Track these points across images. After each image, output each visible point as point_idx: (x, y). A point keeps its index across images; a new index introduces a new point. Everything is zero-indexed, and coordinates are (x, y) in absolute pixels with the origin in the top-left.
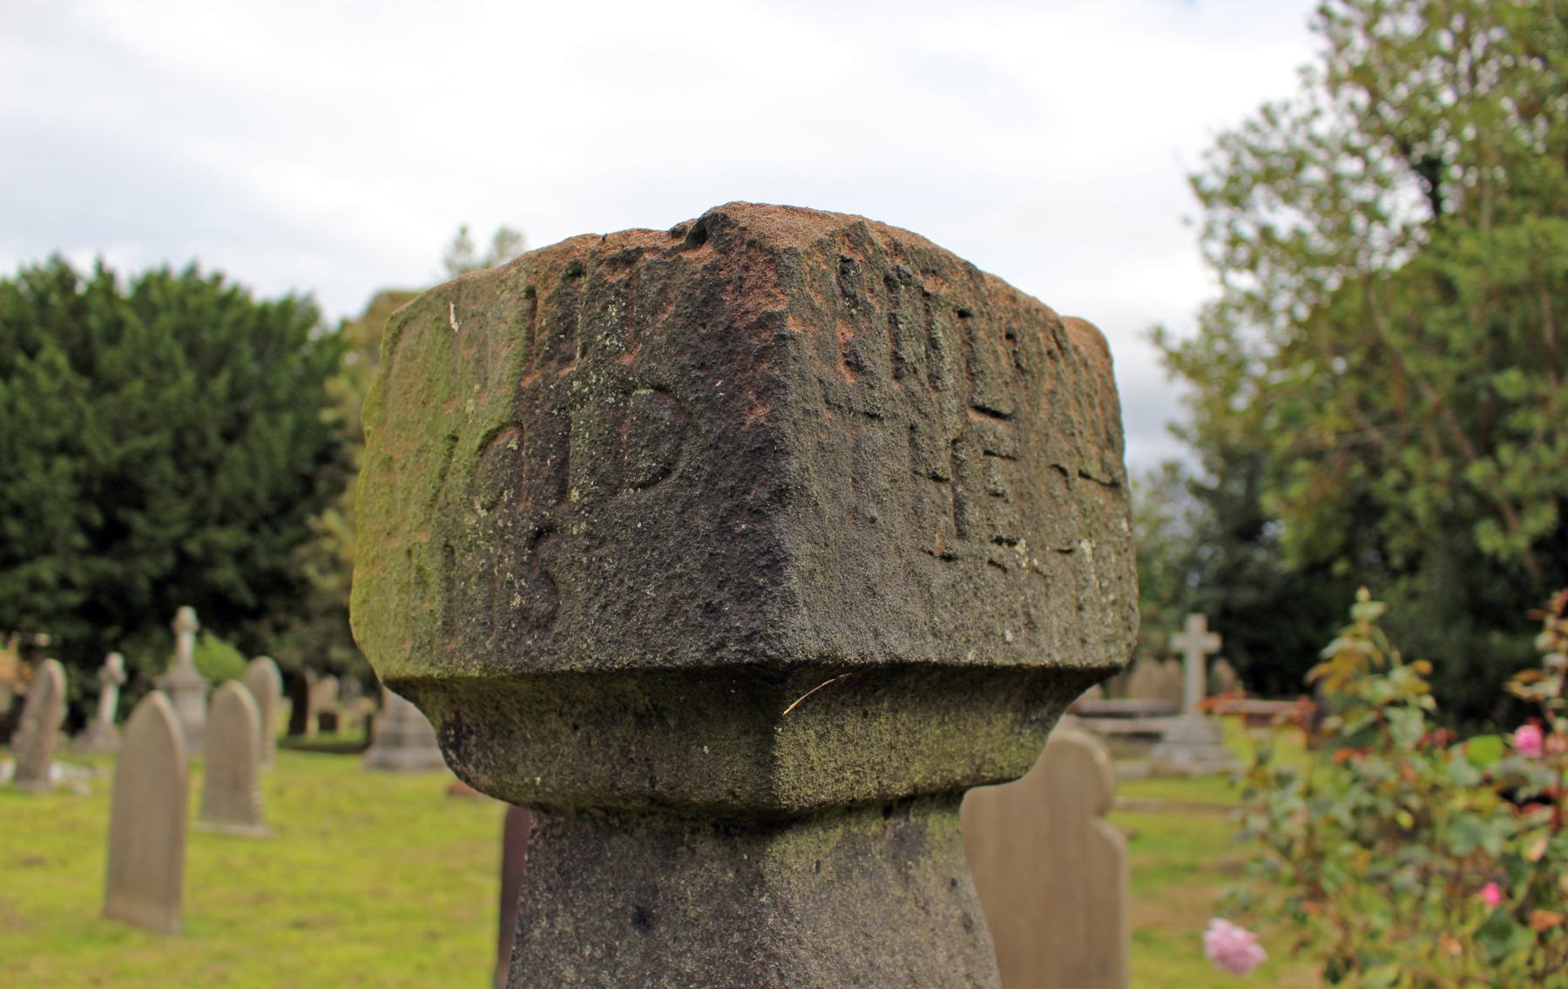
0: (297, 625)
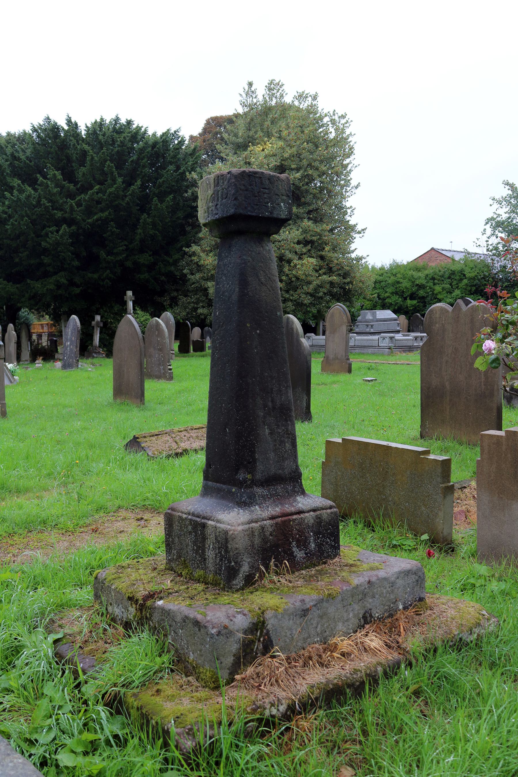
0: (183, 300)
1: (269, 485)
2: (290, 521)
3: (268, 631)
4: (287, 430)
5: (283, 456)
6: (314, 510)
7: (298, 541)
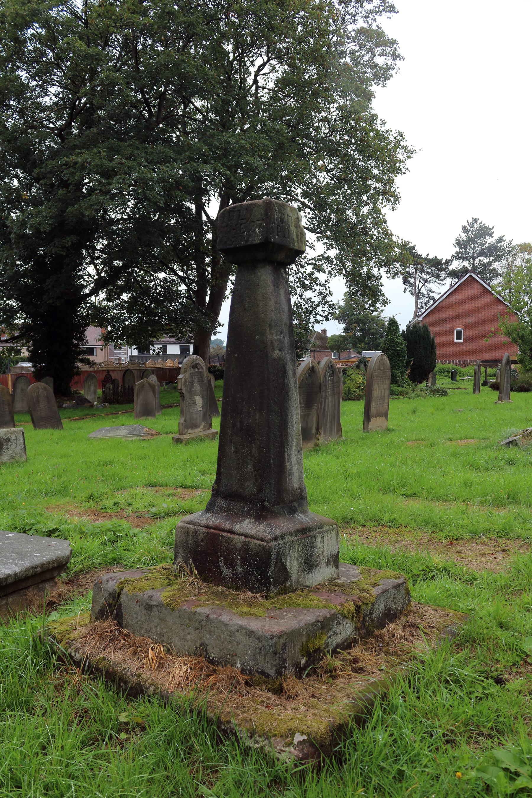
1: (231, 500)
2: (219, 535)
3: (121, 604)
4: (251, 453)
5: (244, 477)
6: (246, 536)
7: (225, 558)
